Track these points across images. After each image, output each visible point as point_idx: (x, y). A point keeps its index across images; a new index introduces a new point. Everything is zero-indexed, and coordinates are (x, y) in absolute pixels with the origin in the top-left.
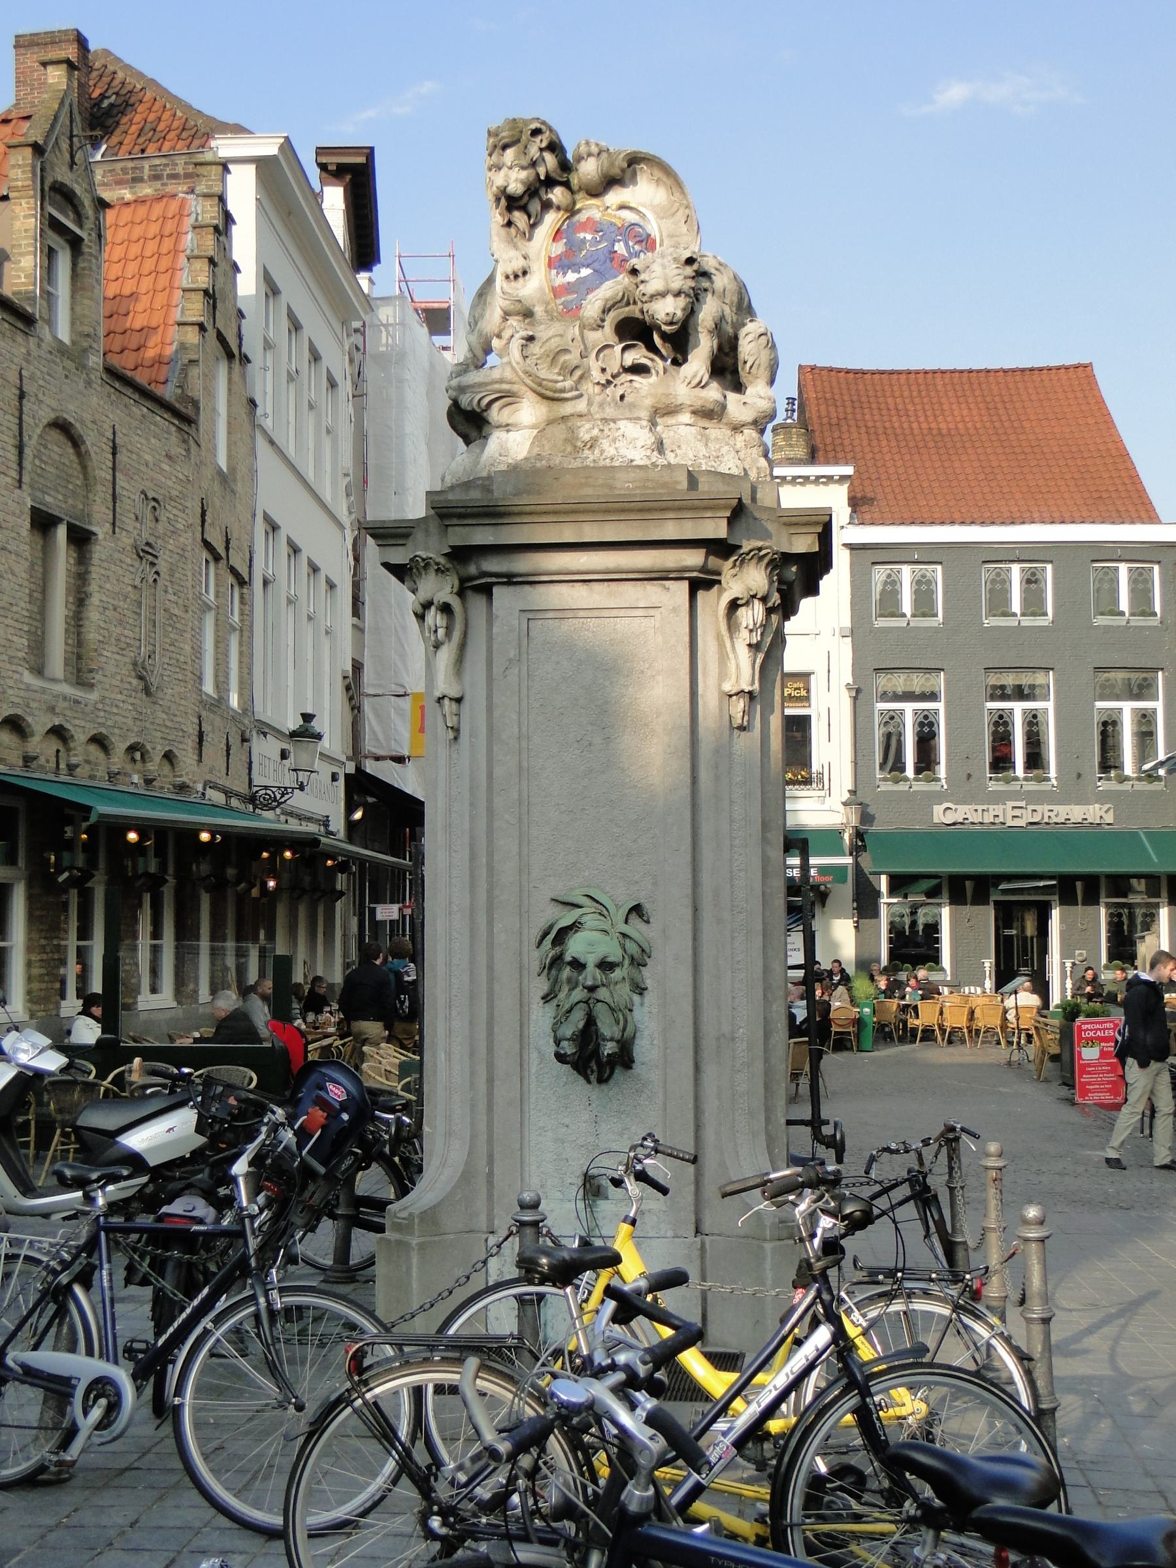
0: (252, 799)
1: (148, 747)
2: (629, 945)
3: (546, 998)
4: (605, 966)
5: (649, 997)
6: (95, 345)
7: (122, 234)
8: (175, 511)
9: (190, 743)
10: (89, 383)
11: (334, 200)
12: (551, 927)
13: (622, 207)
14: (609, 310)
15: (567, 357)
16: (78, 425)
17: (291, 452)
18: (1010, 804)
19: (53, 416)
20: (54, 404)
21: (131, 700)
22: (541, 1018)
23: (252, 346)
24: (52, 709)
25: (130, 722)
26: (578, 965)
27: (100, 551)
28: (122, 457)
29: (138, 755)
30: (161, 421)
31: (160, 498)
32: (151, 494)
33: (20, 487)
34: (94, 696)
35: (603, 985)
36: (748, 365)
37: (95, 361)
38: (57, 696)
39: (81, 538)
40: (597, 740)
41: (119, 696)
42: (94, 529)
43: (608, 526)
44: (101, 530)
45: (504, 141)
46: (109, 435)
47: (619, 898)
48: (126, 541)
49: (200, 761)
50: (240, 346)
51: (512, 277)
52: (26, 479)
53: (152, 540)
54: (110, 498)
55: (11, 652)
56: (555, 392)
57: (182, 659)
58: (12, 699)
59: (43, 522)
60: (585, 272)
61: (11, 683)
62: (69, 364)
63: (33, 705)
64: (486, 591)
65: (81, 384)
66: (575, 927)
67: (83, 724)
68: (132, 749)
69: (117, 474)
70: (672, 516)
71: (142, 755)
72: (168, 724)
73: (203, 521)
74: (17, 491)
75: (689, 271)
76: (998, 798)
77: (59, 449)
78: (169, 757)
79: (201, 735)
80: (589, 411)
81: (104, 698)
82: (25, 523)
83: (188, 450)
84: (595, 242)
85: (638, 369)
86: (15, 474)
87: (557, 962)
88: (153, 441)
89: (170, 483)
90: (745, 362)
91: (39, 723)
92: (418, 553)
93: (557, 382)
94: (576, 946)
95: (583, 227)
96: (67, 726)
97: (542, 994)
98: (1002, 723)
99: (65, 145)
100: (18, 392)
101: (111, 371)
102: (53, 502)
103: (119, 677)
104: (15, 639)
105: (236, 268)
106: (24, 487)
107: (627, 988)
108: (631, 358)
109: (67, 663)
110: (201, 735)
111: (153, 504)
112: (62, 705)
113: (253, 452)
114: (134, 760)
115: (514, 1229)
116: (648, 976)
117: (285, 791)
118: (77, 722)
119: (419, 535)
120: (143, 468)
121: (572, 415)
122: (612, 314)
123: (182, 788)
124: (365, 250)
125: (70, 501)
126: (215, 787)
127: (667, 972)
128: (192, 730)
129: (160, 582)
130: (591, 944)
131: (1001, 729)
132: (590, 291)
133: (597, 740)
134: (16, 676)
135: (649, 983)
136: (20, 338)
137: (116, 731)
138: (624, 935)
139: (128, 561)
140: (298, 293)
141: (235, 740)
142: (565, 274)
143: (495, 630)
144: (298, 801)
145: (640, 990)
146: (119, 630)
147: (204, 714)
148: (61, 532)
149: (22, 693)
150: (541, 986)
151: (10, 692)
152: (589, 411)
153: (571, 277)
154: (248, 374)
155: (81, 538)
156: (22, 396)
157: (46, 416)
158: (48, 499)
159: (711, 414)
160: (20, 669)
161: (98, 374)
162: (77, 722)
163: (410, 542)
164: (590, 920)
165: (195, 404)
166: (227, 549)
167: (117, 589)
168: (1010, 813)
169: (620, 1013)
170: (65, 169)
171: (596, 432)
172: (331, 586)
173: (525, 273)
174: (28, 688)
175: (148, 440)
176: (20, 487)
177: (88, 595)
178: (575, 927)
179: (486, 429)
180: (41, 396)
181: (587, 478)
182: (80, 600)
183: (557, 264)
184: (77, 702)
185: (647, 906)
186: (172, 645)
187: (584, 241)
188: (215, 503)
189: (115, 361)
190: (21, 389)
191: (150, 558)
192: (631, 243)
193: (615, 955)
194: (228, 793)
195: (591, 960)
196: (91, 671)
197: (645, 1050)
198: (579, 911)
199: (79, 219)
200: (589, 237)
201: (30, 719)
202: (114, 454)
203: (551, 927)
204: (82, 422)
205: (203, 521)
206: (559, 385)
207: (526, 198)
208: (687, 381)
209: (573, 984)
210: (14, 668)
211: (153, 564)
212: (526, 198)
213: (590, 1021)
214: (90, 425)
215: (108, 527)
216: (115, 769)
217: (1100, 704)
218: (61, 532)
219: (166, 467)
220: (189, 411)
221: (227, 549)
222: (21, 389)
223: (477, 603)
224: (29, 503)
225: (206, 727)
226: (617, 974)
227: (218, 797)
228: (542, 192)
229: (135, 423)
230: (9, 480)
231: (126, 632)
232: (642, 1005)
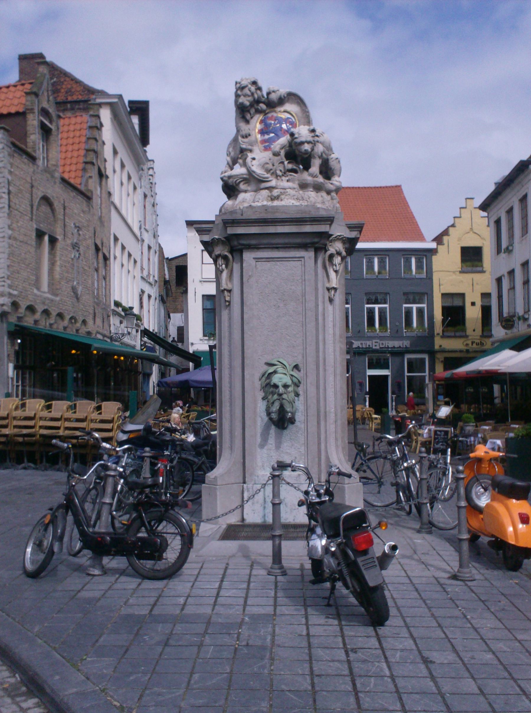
0: (111, 338)
1: (77, 317)
2: (294, 379)
3: (263, 399)
4: (286, 386)
5: (301, 398)
6: (57, 169)
7: (66, 128)
8: (85, 232)
9: (91, 316)
10: (55, 183)
11: (135, 120)
12: (265, 373)
13: (285, 111)
16: (51, 198)
17: (124, 212)
18: (374, 341)
19: (43, 194)
20: (44, 190)
21: (71, 300)
22: (262, 406)
23: (109, 172)
24: (44, 303)
25: (71, 308)
26: (276, 386)
27: (59, 245)
28: (67, 211)
29: (73, 321)
30: (80, 198)
31: (80, 226)
32: (77, 225)
33: (32, 221)
34: (58, 299)
35: (285, 393)
37: (57, 175)
38: (45, 298)
39: (53, 241)
40: (282, 305)
41: (68, 299)
42: (58, 237)
44: (60, 237)
46: (62, 202)
47: (289, 362)
48: (69, 242)
49: (94, 323)
50: (105, 172)
52: (34, 217)
53: (78, 242)
54: (63, 225)
55: (30, 282)
57: (88, 286)
58: (31, 299)
59: (40, 234)
60: (272, 135)
61: (29, 293)
62: (48, 175)
63: (38, 301)
64: (241, 252)
65: (53, 183)
66: (275, 372)
67: (55, 308)
68: (71, 318)
69: (66, 218)
71: (75, 321)
72: (84, 309)
73: (95, 236)
74: (31, 222)
75: (313, 134)
76: (370, 338)
77: (45, 208)
78: (84, 322)
79: (95, 314)
81: (62, 299)
82: (34, 234)
83: (90, 209)
84: (275, 124)
85: (295, 171)
86: (30, 216)
87: (268, 385)
88: (78, 205)
89: (83, 221)
91: (40, 308)
94: (276, 379)
95: (271, 119)
96: (50, 309)
97: (262, 397)
98: (371, 312)
99: (46, 94)
100: (30, 185)
101: (63, 180)
102: (43, 227)
103: (67, 292)
104: (31, 276)
105: (104, 143)
106: (34, 220)
107: (293, 395)
108: (290, 166)
109: (49, 286)
110: (95, 314)
111: (78, 228)
112: (47, 302)
113: (110, 211)
114: (72, 323)
115: (270, 478)
116: (300, 390)
117: (123, 335)
118: (53, 308)
120: (74, 215)
123: (89, 333)
124: (144, 139)
125: (49, 226)
126: (99, 333)
127: (309, 387)
128: (92, 312)
129: (81, 258)
130: (281, 379)
131: (371, 314)
132: (274, 141)
133: (282, 305)
134: (31, 290)
135: (301, 393)
136: (31, 165)
137: (66, 312)
138: (292, 375)
139: (70, 249)
140: (123, 154)
141: (105, 316)
142: (264, 136)
143: (244, 265)
144: (126, 340)
145: (297, 395)
146: (66, 275)
147: (96, 306)
148: (46, 238)
149: (33, 297)
150: (262, 394)
151: (29, 296)
153: (266, 137)
154: (108, 183)
155: (53, 241)
156: (32, 187)
157: (40, 195)
158: (42, 225)
159: (318, 188)
160: (33, 288)
161: (58, 180)
162: (53, 308)
163: (211, 233)
164: (280, 370)
165: (92, 192)
166: (102, 246)
167: (66, 259)
168: (374, 344)
169: (292, 403)
170: (46, 103)
172: (135, 262)
173: (249, 135)
174: (36, 295)
175: (76, 205)
176: (32, 221)
177: (55, 261)
178: (275, 372)
179: (236, 193)
180: (39, 187)
182: (52, 263)
183: (262, 132)
184: (52, 300)
185: (301, 366)
186: (85, 280)
187: (271, 124)
188: (98, 229)
189: (66, 176)
190: (31, 184)
191: (77, 248)
193: (289, 382)
194: (104, 336)
195: (280, 384)
196: (57, 289)
197: (299, 417)
198: (275, 367)
199: (51, 122)
200: (273, 122)
201: (36, 307)
202: (64, 210)
203: (265, 373)
204: (53, 197)
205: (95, 236)
209: (273, 393)
210: (31, 287)
211: (78, 251)
213: (282, 406)
214: (56, 198)
215: (62, 236)
216: (66, 325)
217: (405, 305)
218: (46, 238)
219: (82, 215)
220: (89, 194)
221: (102, 246)
222: (31, 184)
223: (237, 256)
224: (35, 226)
225: (97, 311)
226: (290, 389)
227: (100, 337)
228: (255, 106)
229: (71, 199)
230: (28, 218)
231: (69, 275)
232: (298, 400)
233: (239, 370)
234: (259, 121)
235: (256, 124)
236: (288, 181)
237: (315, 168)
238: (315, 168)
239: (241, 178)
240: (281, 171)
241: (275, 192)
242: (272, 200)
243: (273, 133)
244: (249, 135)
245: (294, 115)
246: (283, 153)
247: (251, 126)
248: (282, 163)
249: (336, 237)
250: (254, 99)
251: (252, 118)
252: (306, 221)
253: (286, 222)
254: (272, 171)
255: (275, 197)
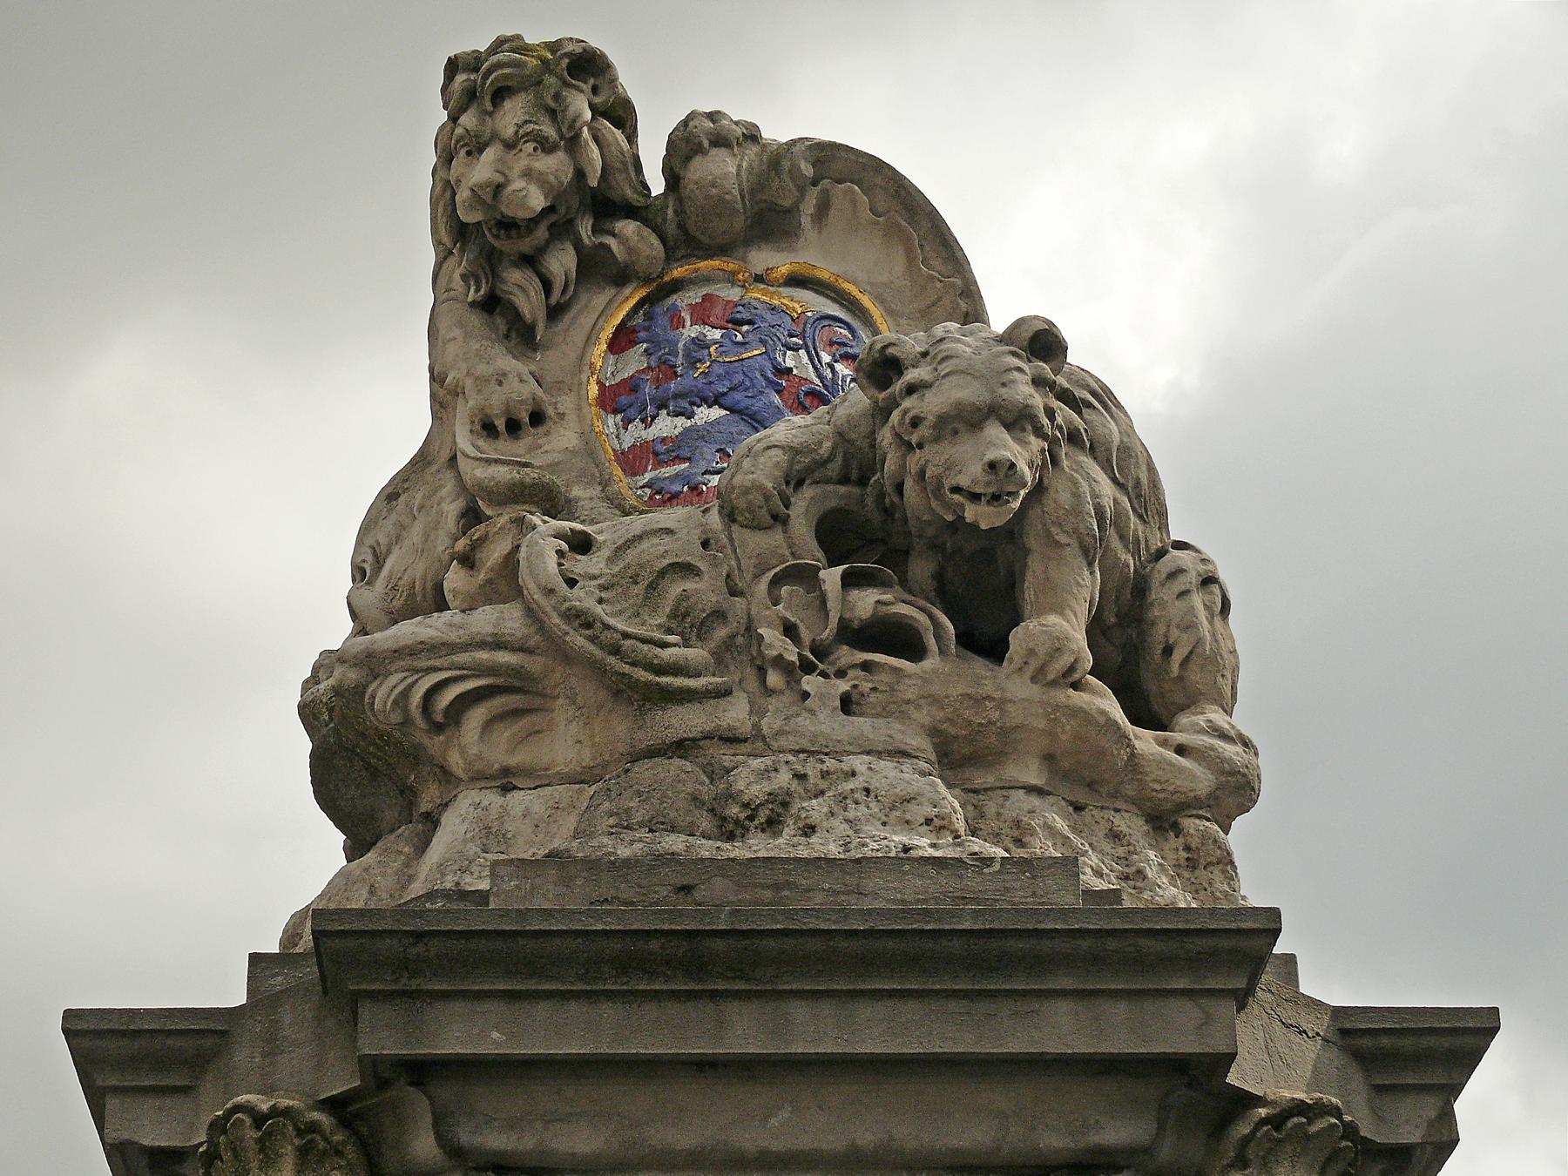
13: (797, 281)
14: (800, 483)
15: (690, 585)
36: (1178, 656)
43: (866, 1011)
45: (478, 84)
51: (500, 424)
56: (660, 670)
60: (707, 414)
70: (1067, 983)
80: (756, 727)
90: (1168, 651)
92: (242, 1098)
93: (664, 645)
108: (866, 602)
119: (245, 1055)
121: (708, 737)
122: (808, 492)
152: (756, 727)
171: (784, 778)
173: (537, 418)
181: (777, 887)
192: (826, 358)
206: (667, 654)
207: (542, 233)
208: (1034, 663)
212: (542, 233)
233: (1427, 1042)
234: (608, 332)
235: (588, 349)
236: (847, 704)
237: (1061, 623)
238: (1061, 623)
239: (480, 670)
240: (790, 630)
241: (751, 779)
242: (730, 831)
243: (716, 401)
244: (537, 418)
245: (866, 301)
246: (803, 508)
247: (555, 360)
248: (804, 576)
249: (1277, 1121)
250: (580, 174)
251: (555, 312)
252: (1039, 964)
253: (864, 964)
254: (721, 633)
255: (752, 809)
